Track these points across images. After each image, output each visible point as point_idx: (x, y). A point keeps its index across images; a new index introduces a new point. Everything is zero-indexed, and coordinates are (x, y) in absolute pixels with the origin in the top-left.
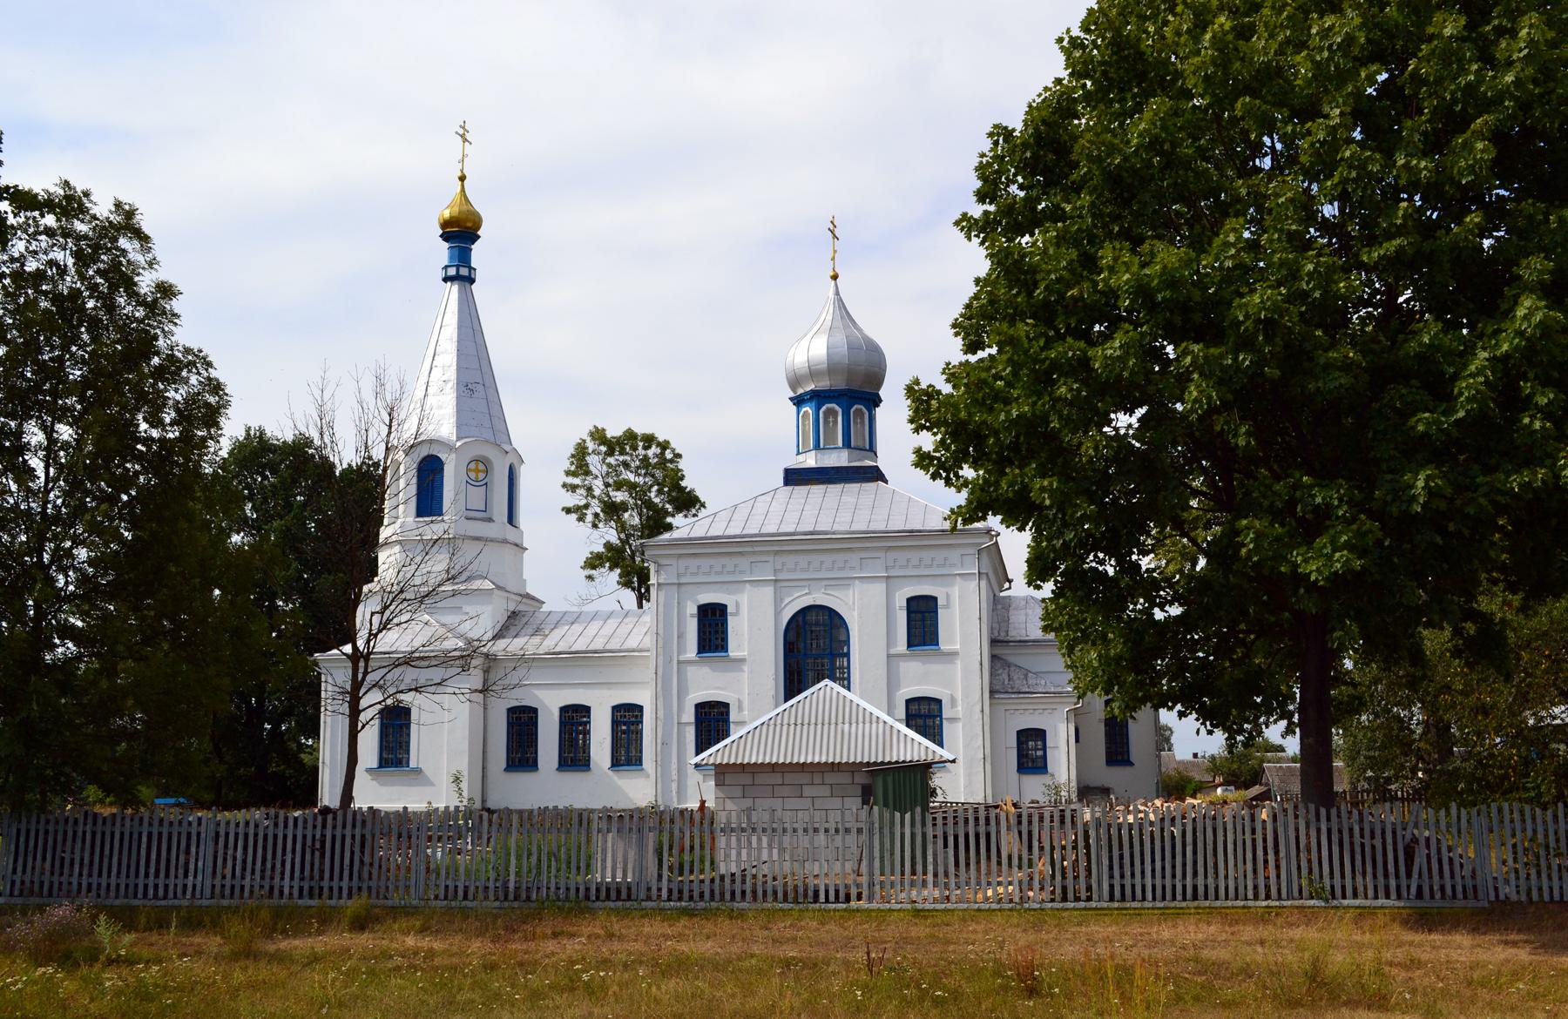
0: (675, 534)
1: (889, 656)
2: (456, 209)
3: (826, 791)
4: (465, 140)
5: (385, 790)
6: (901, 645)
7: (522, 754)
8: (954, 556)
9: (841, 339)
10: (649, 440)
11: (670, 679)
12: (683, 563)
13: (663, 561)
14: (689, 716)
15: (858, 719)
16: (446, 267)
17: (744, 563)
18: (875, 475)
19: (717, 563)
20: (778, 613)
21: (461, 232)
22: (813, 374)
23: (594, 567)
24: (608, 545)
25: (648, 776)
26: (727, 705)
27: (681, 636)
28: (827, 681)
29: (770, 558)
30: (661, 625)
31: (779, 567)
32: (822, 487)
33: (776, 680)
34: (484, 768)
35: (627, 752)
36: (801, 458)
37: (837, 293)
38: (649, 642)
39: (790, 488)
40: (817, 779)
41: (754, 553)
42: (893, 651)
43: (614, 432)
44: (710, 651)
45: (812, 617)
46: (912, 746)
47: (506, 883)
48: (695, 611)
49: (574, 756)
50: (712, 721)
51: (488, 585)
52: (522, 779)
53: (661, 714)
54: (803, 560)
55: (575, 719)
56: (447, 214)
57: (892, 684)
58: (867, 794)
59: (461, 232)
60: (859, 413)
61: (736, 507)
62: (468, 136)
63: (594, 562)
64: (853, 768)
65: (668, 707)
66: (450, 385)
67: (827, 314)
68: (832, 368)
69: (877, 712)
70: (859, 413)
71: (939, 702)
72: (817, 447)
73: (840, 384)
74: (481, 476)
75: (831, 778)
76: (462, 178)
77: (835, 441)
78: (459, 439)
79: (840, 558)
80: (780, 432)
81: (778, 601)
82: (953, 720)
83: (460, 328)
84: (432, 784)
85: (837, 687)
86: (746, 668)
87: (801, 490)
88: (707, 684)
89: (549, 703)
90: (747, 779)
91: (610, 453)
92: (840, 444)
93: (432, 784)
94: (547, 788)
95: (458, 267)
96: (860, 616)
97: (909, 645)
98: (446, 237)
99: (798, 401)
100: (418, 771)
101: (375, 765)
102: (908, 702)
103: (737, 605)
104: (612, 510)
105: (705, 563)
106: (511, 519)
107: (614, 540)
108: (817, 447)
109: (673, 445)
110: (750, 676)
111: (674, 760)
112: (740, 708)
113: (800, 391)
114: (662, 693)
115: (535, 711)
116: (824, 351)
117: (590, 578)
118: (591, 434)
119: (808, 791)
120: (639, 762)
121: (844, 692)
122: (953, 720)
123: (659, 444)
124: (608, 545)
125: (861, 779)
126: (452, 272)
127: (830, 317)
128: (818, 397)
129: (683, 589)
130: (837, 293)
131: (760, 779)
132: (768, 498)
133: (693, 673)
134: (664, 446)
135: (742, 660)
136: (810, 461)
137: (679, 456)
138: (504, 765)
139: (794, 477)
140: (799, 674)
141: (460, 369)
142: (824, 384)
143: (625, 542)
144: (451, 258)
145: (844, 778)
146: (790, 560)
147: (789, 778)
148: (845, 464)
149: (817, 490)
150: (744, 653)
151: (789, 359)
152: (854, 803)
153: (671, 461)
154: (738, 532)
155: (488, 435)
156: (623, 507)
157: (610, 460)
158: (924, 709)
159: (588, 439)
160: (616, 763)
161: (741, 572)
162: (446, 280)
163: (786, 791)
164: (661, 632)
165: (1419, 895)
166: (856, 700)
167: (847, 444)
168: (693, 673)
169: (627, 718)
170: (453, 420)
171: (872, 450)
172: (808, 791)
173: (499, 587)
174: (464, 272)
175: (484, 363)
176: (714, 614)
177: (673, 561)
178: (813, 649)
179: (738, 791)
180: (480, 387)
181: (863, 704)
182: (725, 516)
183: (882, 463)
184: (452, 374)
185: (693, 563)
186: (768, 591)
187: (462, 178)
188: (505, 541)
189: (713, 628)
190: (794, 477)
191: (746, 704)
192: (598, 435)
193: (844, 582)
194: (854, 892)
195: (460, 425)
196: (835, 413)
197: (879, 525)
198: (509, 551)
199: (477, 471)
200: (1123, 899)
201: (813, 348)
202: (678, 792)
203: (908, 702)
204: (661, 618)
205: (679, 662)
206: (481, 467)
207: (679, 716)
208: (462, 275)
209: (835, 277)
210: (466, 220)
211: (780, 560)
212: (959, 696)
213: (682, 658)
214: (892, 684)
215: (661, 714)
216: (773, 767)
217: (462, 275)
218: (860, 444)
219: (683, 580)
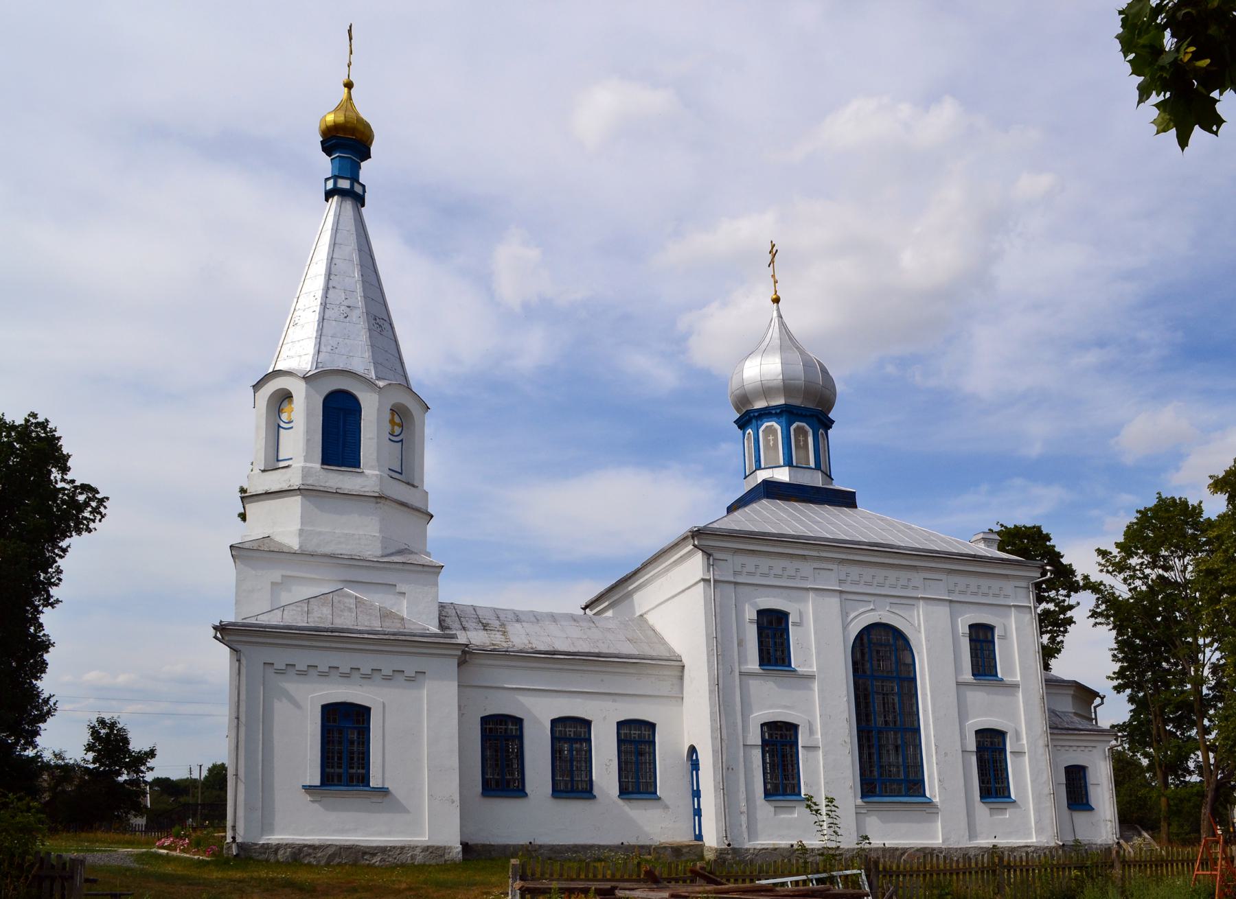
5: (333, 817)
6: (967, 676)
8: (1008, 586)
12: (740, 559)
14: (755, 737)
17: (806, 568)
20: (845, 627)
21: (348, 142)
27: (741, 643)
29: (834, 567)
37: (780, 316)
41: (819, 558)
49: (572, 780)
52: (505, 808)
55: (571, 736)
56: (330, 118)
57: (962, 716)
59: (348, 142)
68: (787, 388)
81: (844, 614)
82: (812, 748)
84: (403, 810)
86: (816, 686)
89: (539, 712)
92: (812, 465)
93: (403, 810)
94: (539, 818)
98: (328, 148)
100: (384, 791)
101: (317, 782)
111: (742, 788)
112: (811, 732)
115: (519, 722)
122: (812, 748)
130: (780, 316)
138: (313, 776)
158: (570, 731)
160: (624, 792)
168: (755, 685)
169: (637, 741)
189: (774, 633)
193: (910, 601)
196: (806, 434)
202: (748, 827)
205: (741, 674)
207: (744, 738)
208: (348, 191)
209: (776, 300)
214: (962, 716)
217: (348, 191)
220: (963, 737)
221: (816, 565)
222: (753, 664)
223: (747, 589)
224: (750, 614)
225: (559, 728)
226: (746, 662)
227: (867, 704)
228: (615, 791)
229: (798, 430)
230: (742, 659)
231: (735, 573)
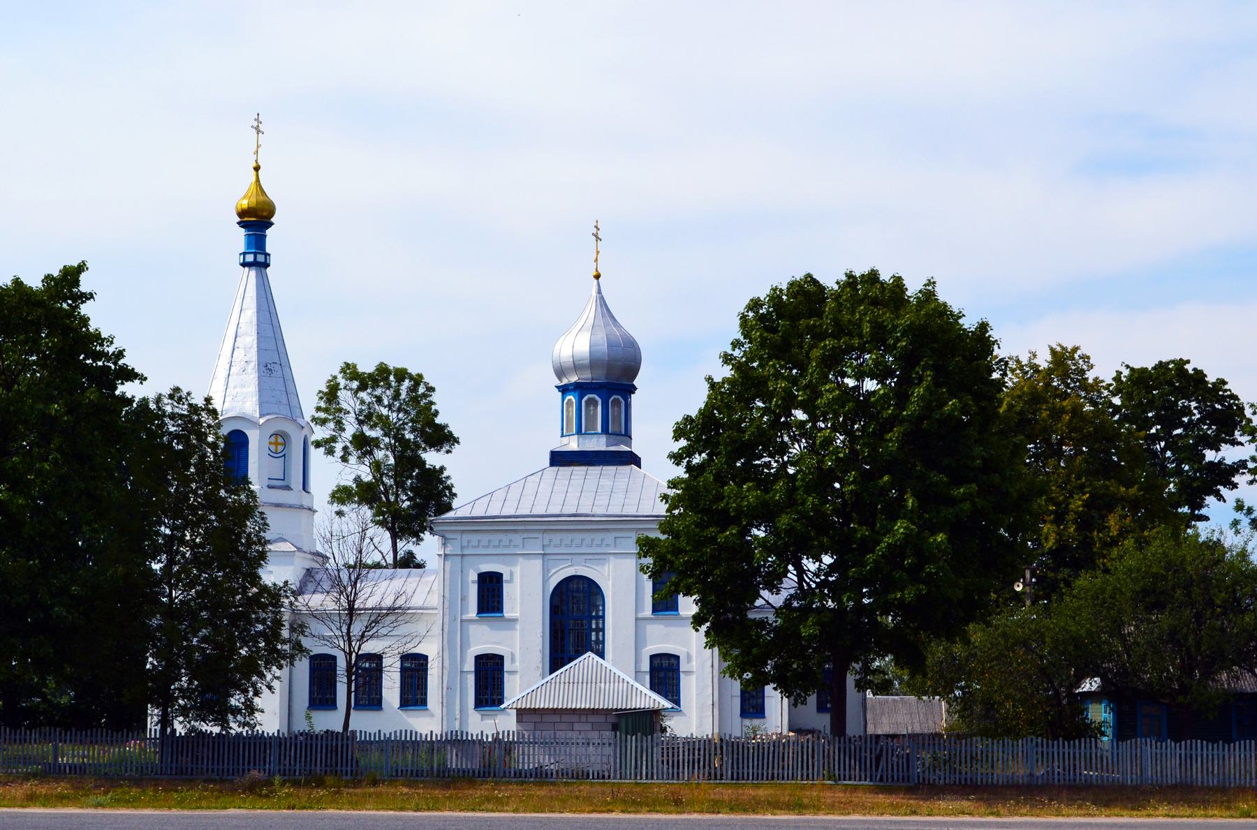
0: (460, 513)
1: (637, 619)
2: (254, 200)
3: (588, 727)
4: (258, 132)
6: (648, 611)
7: (322, 697)
9: (601, 337)
10: (401, 374)
11: (455, 636)
12: (466, 537)
13: (448, 536)
14: (470, 666)
15: (610, 681)
16: (244, 254)
17: (517, 538)
18: (632, 459)
19: (495, 538)
20: (545, 581)
21: (256, 220)
22: (576, 367)
23: (342, 501)
24: (358, 480)
25: (432, 715)
26: (501, 658)
28: (589, 653)
29: (540, 536)
30: (447, 589)
31: (546, 542)
32: (584, 468)
33: (543, 637)
34: (289, 706)
35: (414, 694)
36: (565, 440)
37: (599, 292)
38: (435, 600)
39: (555, 469)
40: (583, 718)
42: (640, 615)
43: (367, 367)
44: (488, 612)
45: (574, 586)
46: (648, 699)
47: (432, 768)
48: (476, 578)
49: (369, 697)
50: (490, 674)
51: (287, 547)
53: (447, 664)
54: (567, 537)
56: (245, 204)
57: (639, 642)
58: (615, 727)
59: (256, 220)
60: (616, 402)
61: (509, 486)
62: (261, 127)
63: (90, 296)
64: (606, 712)
65: (452, 658)
66: (252, 365)
67: (590, 312)
68: (594, 363)
69: (627, 679)
70: (616, 402)
71: (677, 658)
72: (579, 432)
73: (601, 378)
74: (280, 448)
75: (592, 718)
76: (257, 169)
77: (595, 429)
78: (261, 416)
79: (598, 537)
80: (548, 423)
82: (689, 673)
83: (258, 312)
85: (597, 658)
86: (518, 627)
87: (565, 471)
88: (485, 639)
90: (537, 718)
91: (363, 387)
92: (599, 430)
95: (255, 254)
96: (614, 586)
97: (655, 610)
99: (564, 390)
102: (653, 657)
103: (512, 574)
104: (363, 444)
105: (485, 538)
106: (305, 487)
107: (367, 477)
108: (579, 432)
109: (426, 379)
110: (522, 636)
112: (513, 660)
113: (565, 381)
114: (448, 645)
116: (587, 349)
117: (340, 513)
118: (343, 371)
119: (576, 726)
120: (423, 702)
121: (600, 660)
122: (689, 673)
123: (411, 378)
124: (358, 480)
125: (611, 719)
126: (250, 258)
127: (592, 315)
128: (580, 389)
129: (466, 559)
130: (599, 292)
131: (547, 718)
132: (536, 478)
133: (473, 629)
134: (417, 380)
135: (515, 620)
136: (573, 444)
137: (432, 389)
138: (307, 704)
139: (559, 459)
140: (562, 632)
141: (260, 350)
142: (586, 376)
143: (379, 481)
144: (248, 245)
145: (601, 719)
146: (556, 538)
147: (565, 718)
148: (603, 448)
149: (579, 471)
150: (516, 614)
151: (556, 352)
152: (608, 734)
153: (425, 396)
154: (512, 513)
155: (286, 411)
156: (375, 443)
157: (363, 395)
158: (665, 663)
159: (340, 376)
161: (515, 546)
162: (244, 265)
163: (563, 726)
164: (447, 595)
165: (881, 780)
166: (610, 667)
167: (605, 430)
168: (473, 629)
169: (415, 668)
170: (255, 398)
171: (627, 435)
172: (576, 726)
173: (299, 549)
174: (261, 258)
175: (279, 343)
176: (491, 581)
177: (458, 536)
178: (574, 621)
179: (531, 726)
180: (277, 367)
181: (614, 670)
182: (499, 496)
183: (636, 448)
184: (253, 355)
185: (475, 538)
186: (538, 563)
187: (257, 169)
188: (301, 507)
189: (491, 593)
190: (559, 459)
191: (517, 656)
192: (350, 371)
193: (601, 557)
194: (606, 774)
195: (261, 404)
197: (631, 510)
198: (305, 513)
199: (276, 444)
200: (738, 779)
201: (578, 344)
203: (653, 657)
204: (447, 583)
206: (280, 440)
208: (257, 259)
209: (597, 277)
210: (263, 210)
211: (547, 537)
212: (694, 653)
213: (464, 617)
214: (639, 642)
215: (447, 664)
216: (555, 711)
217: (257, 259)
218: (617, 430)
219: (466, 552)
220: (637, 661)
221: (525, 535)
222: (472, 613)
223: (470, 558)
224: (473, 577)
225: (656, 662)
226: (468, 612)
227: (563, 639)
228: (397, 703)
229: (589, 402)
230: (464, 610)
231: (462, 548)
